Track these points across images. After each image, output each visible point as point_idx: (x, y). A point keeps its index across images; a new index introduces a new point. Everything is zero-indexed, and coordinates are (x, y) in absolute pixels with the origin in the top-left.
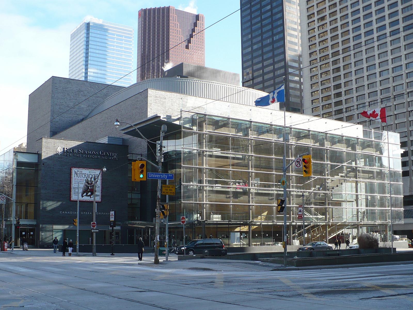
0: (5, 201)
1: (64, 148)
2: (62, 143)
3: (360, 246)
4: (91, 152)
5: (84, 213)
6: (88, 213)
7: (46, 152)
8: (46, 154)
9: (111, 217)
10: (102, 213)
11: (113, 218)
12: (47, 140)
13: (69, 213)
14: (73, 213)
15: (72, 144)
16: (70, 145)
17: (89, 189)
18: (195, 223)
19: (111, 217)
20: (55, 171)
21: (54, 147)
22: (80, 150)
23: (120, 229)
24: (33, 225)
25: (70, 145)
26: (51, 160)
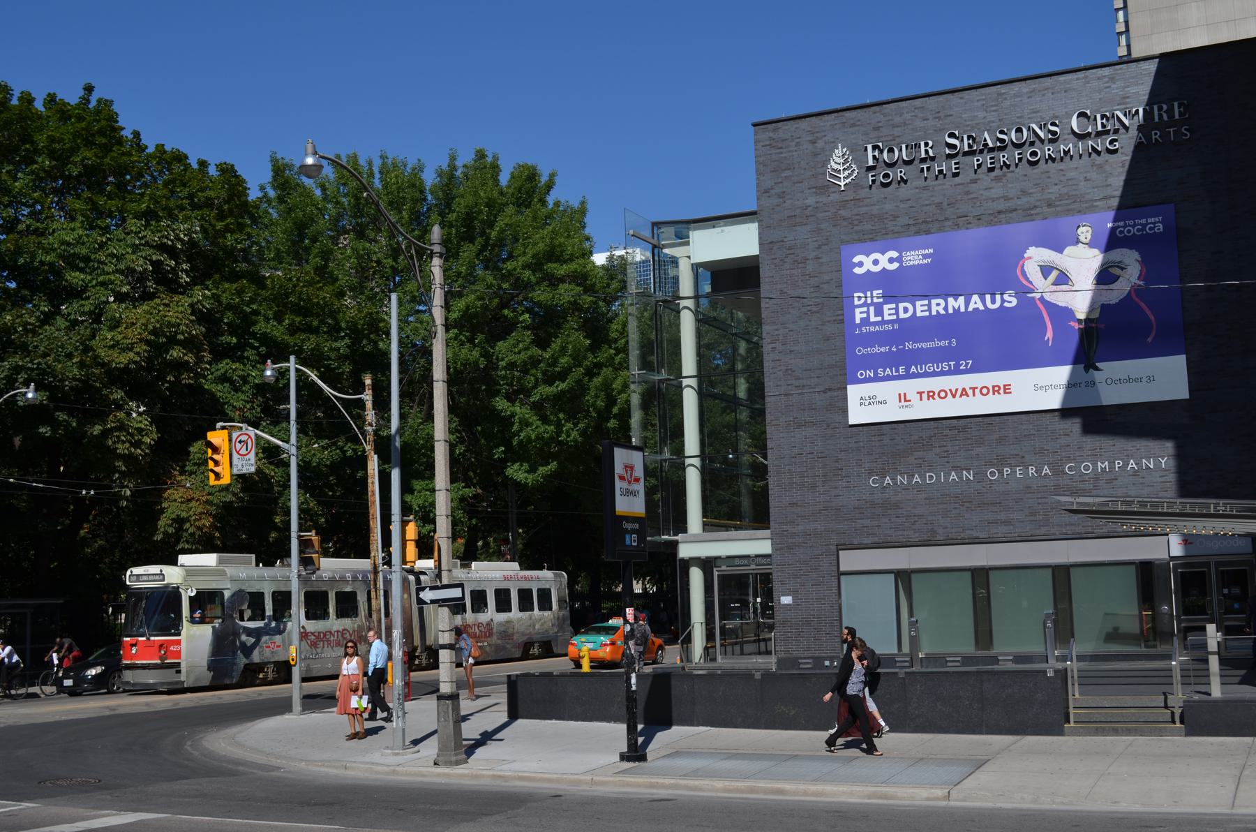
0: (252, 456)
1: (89, 89)
2: (853, 125)
3: (845, 250)
4: (1019, 130)
5: (1007, 471)
6: (1032, 471)
7: (778, 189)
8: (775, 201)
9: (625, 485)
10: (1118, 464)
11: (635, 494)
12: (775, 130)
13: (917, 478)
14: (938, 477)
15: (907, 116)
16: (894, 126)
17: (524, 321)
18: (124, 487)
19: (619, 485)
20: (826, 277)
21: (816, 155)
22: (952, 135)
23: (1250, 550)
24: (748, 557)
25: (894, 126)
26: (802, 224)
